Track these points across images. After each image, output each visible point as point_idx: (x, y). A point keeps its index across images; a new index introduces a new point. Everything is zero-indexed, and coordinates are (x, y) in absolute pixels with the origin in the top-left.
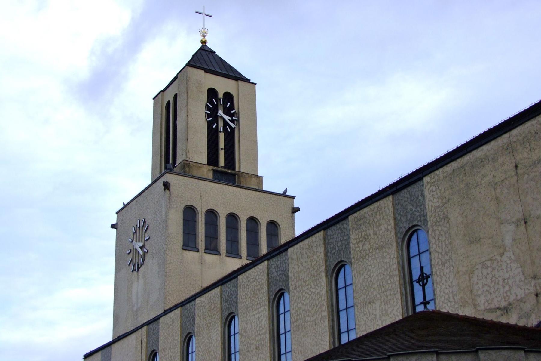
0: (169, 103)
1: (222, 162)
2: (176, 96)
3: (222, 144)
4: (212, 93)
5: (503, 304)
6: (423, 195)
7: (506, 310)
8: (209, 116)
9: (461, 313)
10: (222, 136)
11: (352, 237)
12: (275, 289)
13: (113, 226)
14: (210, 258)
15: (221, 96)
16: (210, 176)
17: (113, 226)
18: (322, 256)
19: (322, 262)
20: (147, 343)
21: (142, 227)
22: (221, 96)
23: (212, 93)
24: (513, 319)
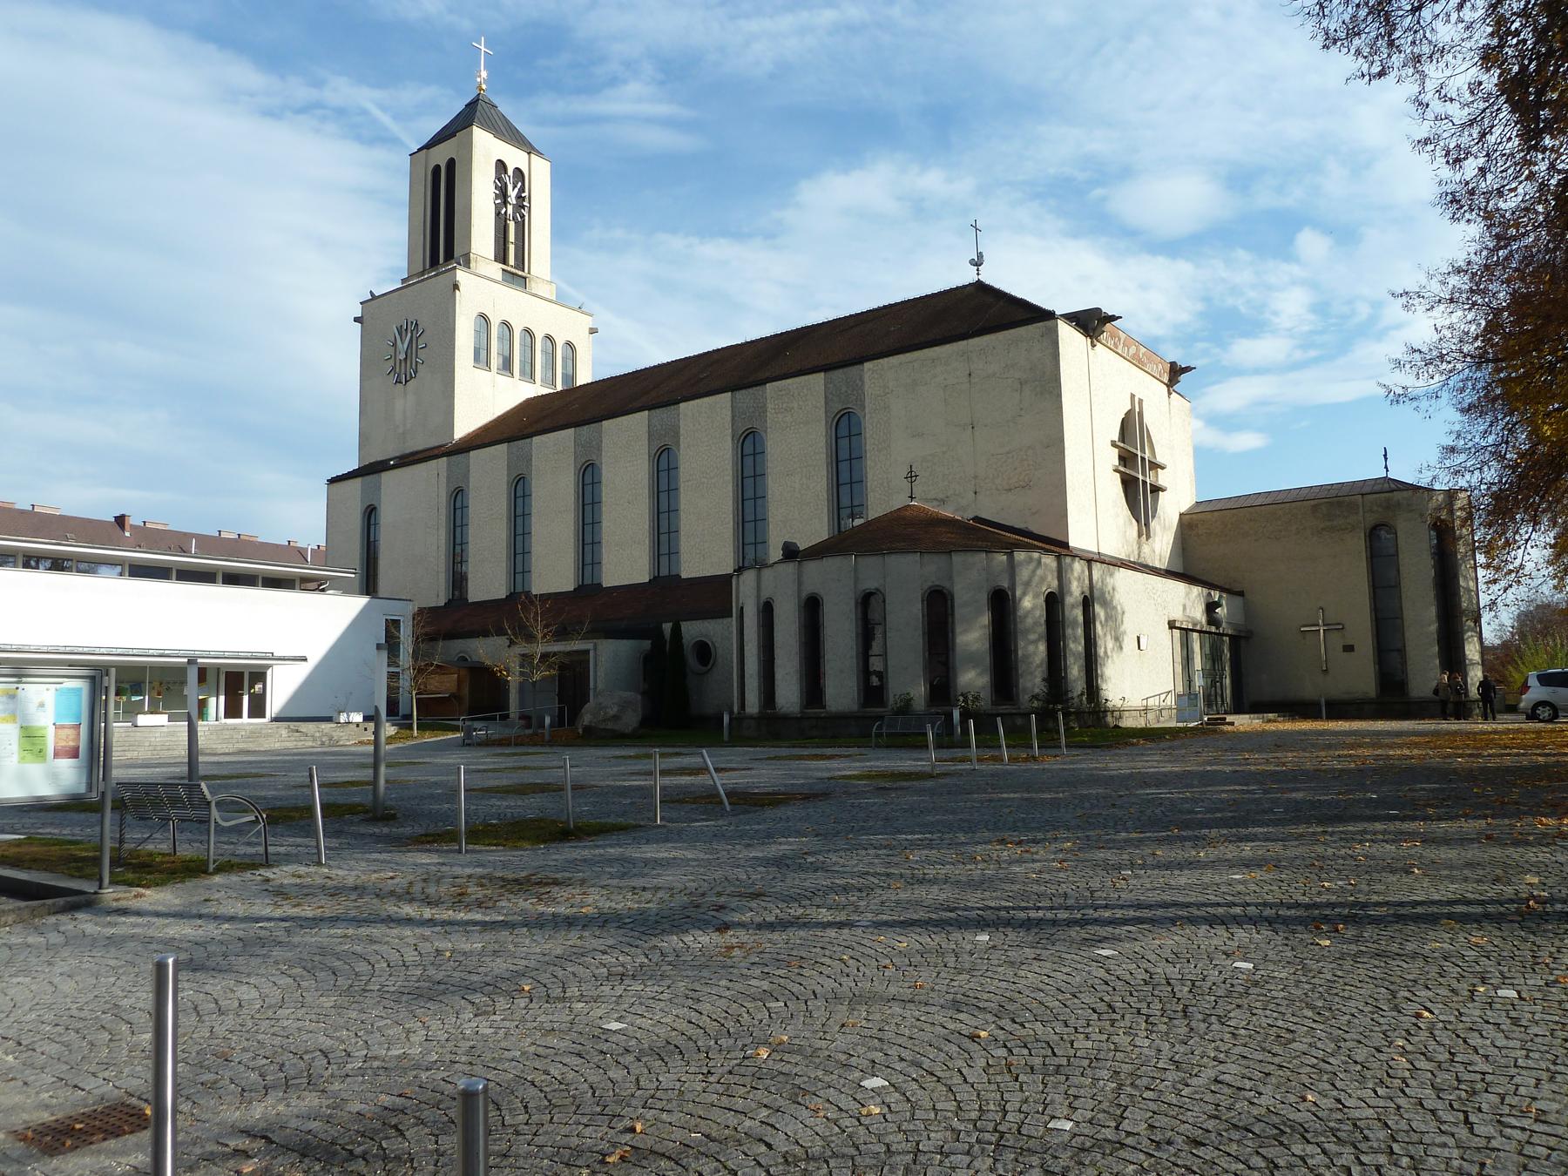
0: (437, 169)
1: (512, 261)
2: (451, 164)
3: (512, 238)
4: (501, 166)
5: (941, 496)
6: (861, 379)
7: (943, 501)
8: (497, 197)
9: (1434, 627)
10: (512, 225)
11: (770, 406)
12: (657, 444)
13: (356, 320)
14: (503, 380)
15: (510, 172)
16: (499, 276)
17: (356, 320)
18: (729, 418)
19: (728, 425)
20: (448, 478)
21: (411, 330)
22: (510, 172)
23: (501, 166)
24: (947, 512)
